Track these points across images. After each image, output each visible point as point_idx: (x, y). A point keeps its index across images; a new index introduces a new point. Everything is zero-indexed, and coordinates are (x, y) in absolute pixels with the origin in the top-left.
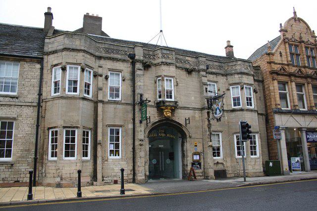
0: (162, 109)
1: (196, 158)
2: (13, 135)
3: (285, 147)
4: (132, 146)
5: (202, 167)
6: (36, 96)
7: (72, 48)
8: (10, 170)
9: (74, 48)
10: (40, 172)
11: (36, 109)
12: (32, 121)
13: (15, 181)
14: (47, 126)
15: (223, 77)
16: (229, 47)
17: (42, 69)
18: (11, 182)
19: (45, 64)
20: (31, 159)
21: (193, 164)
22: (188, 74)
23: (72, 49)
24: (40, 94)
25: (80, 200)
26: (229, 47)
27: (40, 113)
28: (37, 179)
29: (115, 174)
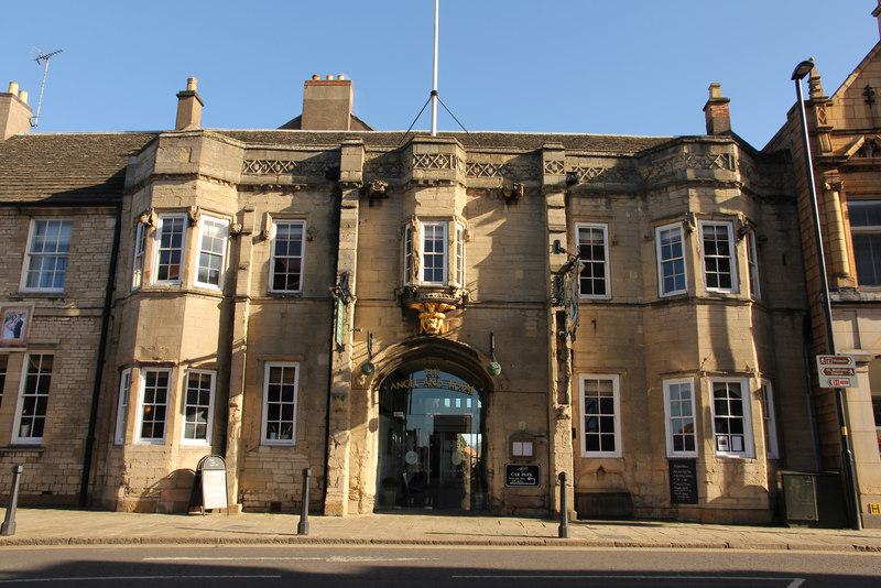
0: (417, 312)
1: (523, 449)
2: (755, 355)
3: (775, 432)
4: (325, 414)
5: (543, 480)
6: (101, 293)
7: (170, 172)
8: (36, 466)
9: (174, 172)
10: (99, 473)
11: (100, 322)
12: (89, 352)
13: (44, 493)
14: (119, 364)
15: (631, 203)
16: (714, 104)
17: (118, 228)
18: (37, 493)
19: (125, 217)
20: (80, 442)
21: (510, 470)
22: (508, 204)
23: (170, 175)
24: (111, 288)
25: (305, 541)
26: (714, 104)
27: (109, 333)
28: (90, 488)
29: (275, 486)
